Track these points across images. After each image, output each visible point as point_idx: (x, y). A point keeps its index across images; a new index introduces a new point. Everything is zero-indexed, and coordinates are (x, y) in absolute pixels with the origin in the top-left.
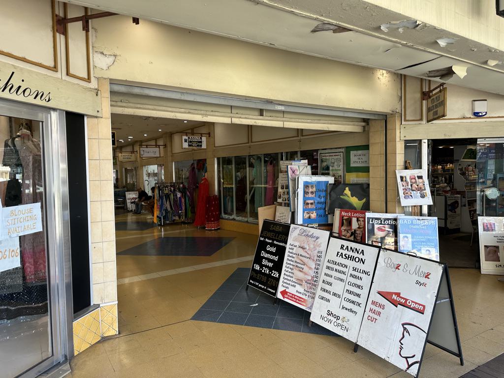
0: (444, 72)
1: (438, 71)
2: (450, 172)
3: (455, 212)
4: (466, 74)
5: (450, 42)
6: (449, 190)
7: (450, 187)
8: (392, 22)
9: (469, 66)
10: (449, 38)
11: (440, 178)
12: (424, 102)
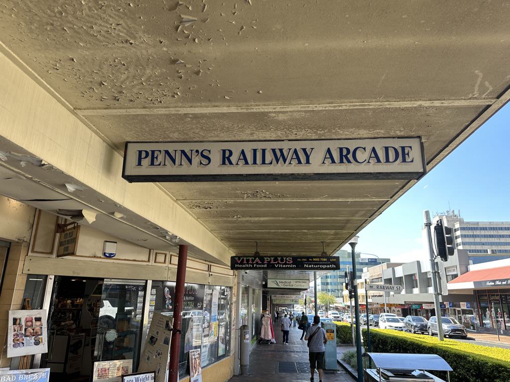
0: (74, 214)
1: (68, 211)
2: (79, 308)
3: (77, 353)
4: (95, 220)
5: (78, 189)
6: (75, 329)
7: (76, 324)
8: (12, 153)
9: (98, 213)
10: (77, 185)
11: (68, 314)
12: (58, 235)
